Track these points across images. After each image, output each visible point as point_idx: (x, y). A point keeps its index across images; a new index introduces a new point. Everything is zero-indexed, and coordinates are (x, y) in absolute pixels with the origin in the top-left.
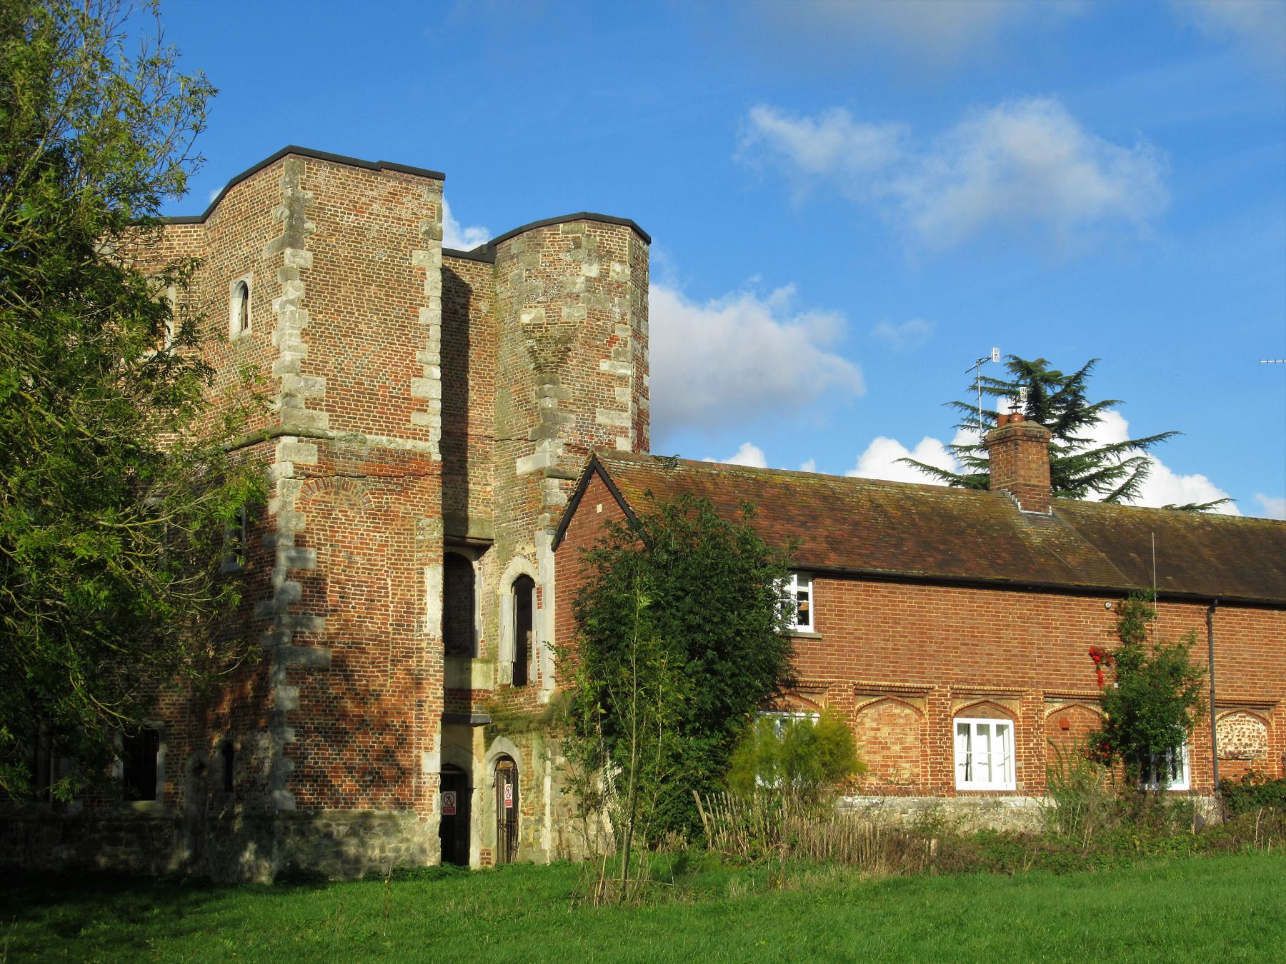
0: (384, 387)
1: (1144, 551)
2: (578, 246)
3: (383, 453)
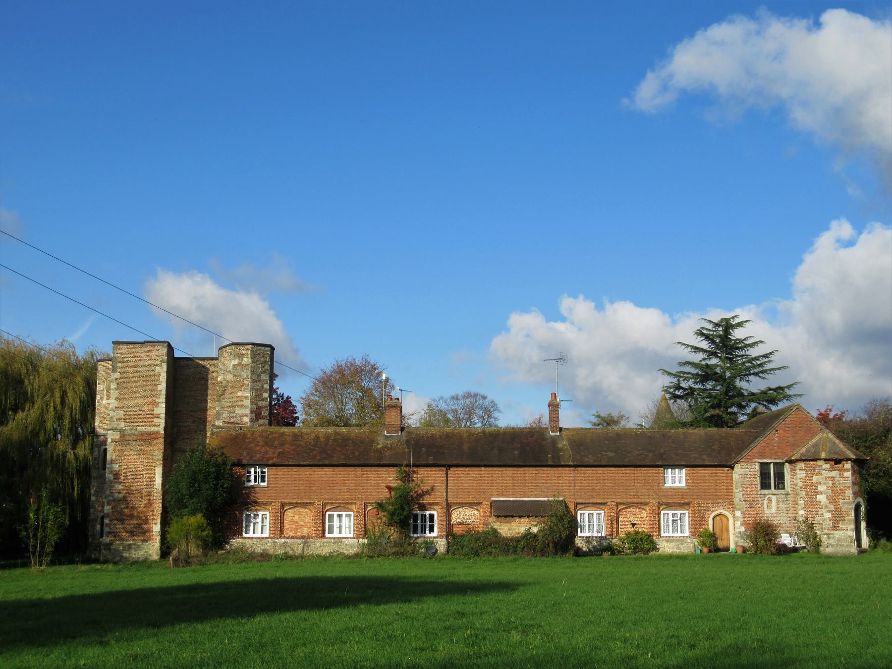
3: (143, 433)
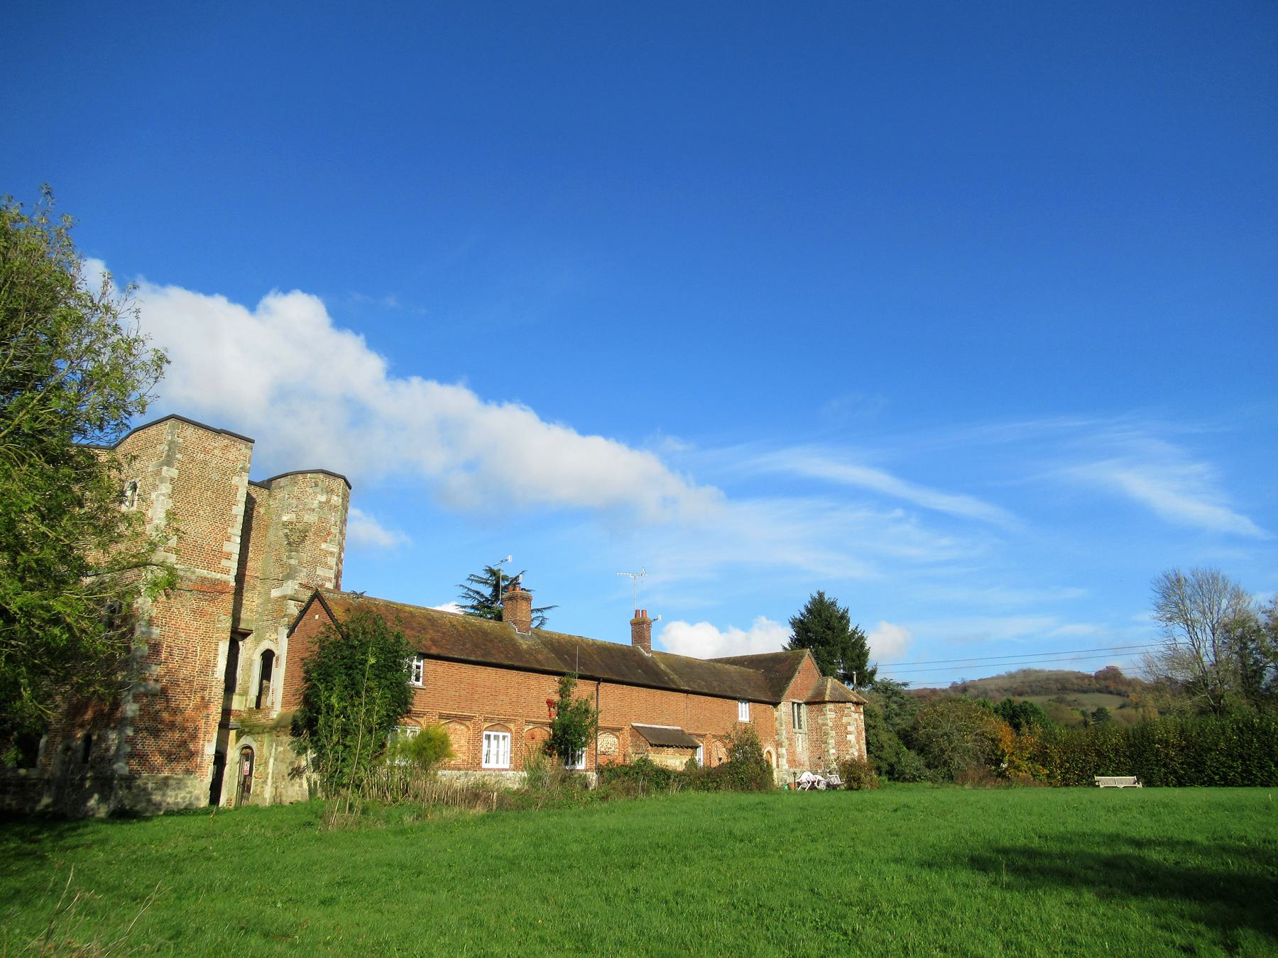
1: (572, 656)
2: (316, 485)
3: (204, 579)
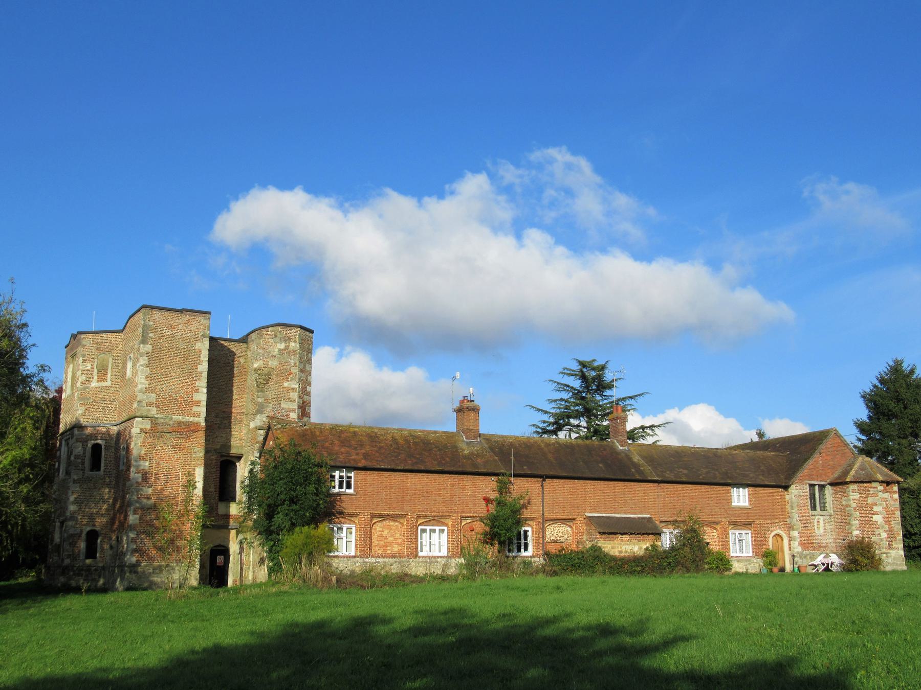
0: (181, 397)
3: (179, 423)
